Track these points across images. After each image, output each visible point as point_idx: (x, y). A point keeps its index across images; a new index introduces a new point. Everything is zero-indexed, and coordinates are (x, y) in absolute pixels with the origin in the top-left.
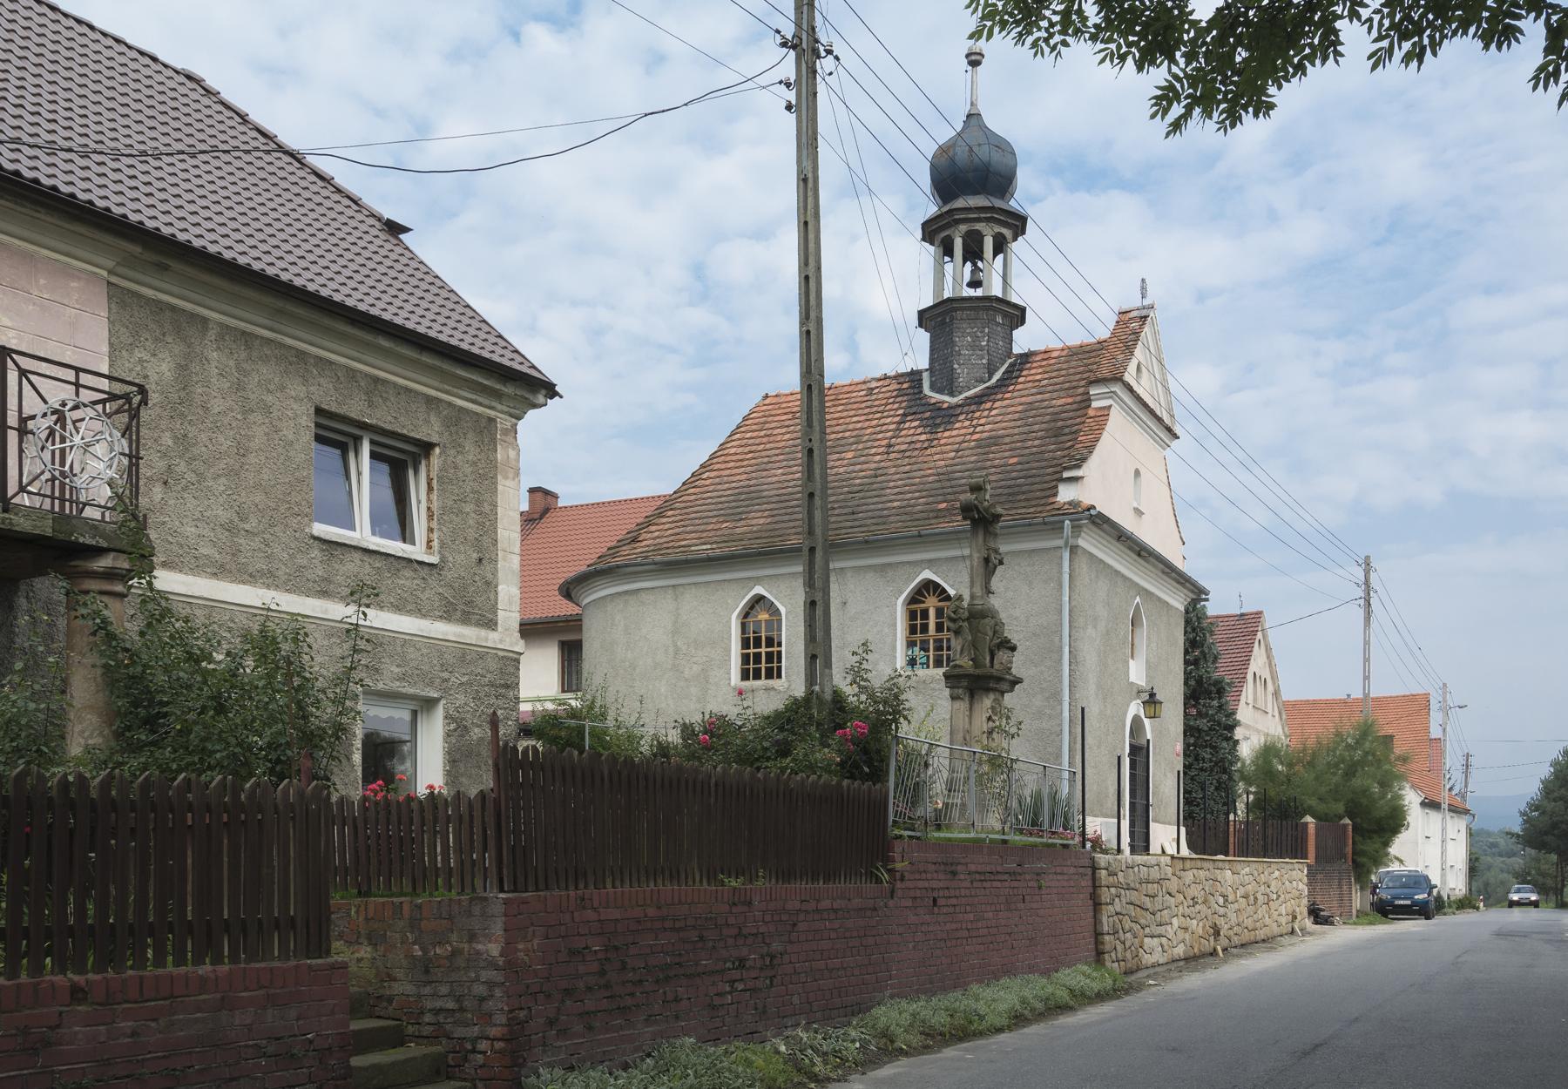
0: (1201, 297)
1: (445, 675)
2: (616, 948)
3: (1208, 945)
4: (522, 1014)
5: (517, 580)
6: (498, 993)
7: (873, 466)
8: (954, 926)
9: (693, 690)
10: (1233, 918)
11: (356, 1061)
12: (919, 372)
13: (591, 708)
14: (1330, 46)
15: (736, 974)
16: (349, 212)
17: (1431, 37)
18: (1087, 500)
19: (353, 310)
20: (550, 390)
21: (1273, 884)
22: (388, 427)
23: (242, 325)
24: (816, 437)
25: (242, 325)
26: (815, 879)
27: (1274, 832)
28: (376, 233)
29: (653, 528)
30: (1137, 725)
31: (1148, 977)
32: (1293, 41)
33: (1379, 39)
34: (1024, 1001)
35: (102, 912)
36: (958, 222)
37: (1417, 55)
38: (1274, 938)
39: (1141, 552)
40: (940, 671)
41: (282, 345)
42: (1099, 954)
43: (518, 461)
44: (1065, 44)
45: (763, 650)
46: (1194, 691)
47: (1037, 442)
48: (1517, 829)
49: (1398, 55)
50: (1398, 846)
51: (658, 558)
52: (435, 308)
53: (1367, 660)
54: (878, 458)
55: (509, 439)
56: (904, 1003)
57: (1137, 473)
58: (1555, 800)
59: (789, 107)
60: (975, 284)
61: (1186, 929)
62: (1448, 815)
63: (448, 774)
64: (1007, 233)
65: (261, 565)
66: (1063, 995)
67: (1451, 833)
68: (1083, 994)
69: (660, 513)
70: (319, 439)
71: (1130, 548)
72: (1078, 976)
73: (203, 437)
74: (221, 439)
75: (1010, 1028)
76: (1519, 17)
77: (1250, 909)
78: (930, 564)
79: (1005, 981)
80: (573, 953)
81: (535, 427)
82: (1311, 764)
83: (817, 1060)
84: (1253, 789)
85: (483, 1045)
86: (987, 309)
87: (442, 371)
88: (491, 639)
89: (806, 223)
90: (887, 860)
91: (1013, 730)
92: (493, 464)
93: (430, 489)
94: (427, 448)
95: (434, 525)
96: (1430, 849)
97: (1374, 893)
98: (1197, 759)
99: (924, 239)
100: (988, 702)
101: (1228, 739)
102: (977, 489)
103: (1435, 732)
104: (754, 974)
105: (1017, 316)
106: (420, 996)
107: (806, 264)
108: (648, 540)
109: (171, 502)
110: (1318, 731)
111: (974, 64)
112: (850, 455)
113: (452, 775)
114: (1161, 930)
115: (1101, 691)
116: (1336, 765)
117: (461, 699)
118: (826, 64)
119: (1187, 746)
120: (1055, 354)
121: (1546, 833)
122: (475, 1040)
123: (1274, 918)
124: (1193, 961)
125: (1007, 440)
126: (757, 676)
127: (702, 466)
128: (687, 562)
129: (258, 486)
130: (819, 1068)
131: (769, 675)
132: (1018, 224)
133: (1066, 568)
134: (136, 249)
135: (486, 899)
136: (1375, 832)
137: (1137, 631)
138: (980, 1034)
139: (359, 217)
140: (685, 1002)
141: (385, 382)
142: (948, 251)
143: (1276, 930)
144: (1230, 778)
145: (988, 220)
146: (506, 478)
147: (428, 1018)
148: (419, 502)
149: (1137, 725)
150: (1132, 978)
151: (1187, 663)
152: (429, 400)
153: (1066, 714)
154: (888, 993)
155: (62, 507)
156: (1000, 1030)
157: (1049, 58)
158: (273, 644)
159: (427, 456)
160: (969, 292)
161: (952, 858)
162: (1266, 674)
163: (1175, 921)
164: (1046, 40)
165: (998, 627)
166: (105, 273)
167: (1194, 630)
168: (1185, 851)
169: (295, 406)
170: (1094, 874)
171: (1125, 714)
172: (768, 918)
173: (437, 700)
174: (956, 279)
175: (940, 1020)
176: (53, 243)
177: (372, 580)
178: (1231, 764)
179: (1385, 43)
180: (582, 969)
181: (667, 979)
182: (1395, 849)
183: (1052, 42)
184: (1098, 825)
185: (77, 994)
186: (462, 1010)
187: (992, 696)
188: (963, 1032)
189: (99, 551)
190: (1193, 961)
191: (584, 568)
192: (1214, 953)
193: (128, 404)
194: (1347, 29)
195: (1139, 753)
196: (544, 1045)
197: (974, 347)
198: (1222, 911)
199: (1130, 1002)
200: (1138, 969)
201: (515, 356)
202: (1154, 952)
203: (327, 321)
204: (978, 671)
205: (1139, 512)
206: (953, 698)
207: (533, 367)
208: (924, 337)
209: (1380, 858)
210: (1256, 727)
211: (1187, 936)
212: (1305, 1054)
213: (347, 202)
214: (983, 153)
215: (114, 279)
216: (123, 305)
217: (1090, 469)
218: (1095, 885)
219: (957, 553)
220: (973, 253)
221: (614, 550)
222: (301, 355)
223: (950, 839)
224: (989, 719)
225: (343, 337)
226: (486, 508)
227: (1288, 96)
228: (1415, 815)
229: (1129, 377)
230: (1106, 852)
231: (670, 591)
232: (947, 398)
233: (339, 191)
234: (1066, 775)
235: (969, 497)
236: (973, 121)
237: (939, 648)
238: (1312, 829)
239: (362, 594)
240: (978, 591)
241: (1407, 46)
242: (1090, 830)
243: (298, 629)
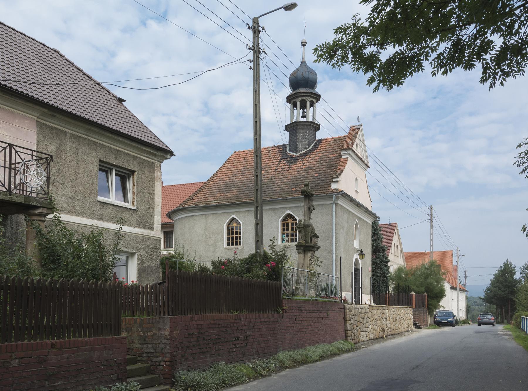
0: (375, 115)
1: (138, 245)
2: (202, 333)
3: (381, 335)
4: (175, 354)
5: (160, 214)
6: (168, 347)
7: (271, 176)
8: (301, 327)
9: (211, 249)
10: (389, 326)
11: (128, 368)
12: (285, 145)
13: (179, 255)
14: (420, 67)
15: (236, 342)
16: (107, 95)
17: (450, 67)
18: (341, 188)
19: (112, 129)
20: (172, 154)
21: (402, 314)
22: (121, 166)
23: (77, 134)
24: (259, 172)
25: (77, 134)
26: (259, 312)
27: (402, 297)
28: (115, 102)
29: (198, 195)
30: (357, 262)
31: (362, 345)
32: (409, 66)
33: (435, 68)
34: (324, 352)
35: (48, 322)
37: (445, 72)
38: (402, 333)
39: (358, 205)
40: (294, 244)
41: (89, 140)
42: (346, 337)
43: (161, 176)
44: (342, 65)
45: (235, 236)
46: (375, 250)
47: (324, 169)
48: (483, 297)
49: (440, 72)
50: (443, 302)
51: (200, 205)
52: (117, 117)
53: (431, 240)
54: (272, 173)
55: (159, 169)
56: (286, 352)
57: (356, 179)
58: (495, 287)
59: (251, 68)
60: (304, 117)
61: (374, 329)
62: (459, 292)
63: (138, 277)
64: (314, 100)
65: (82, 210)
66: (336, 350)
67: (460, 298)
68: (342, 350)
69: (200, 190)
70: (100, 170)
71: (354, 204)
72: (340, 344)
73: (65, 169)
74: (70, 170)
75: (320, 360)
76: (474, 61)
77: (394, 323)
78: (290, 208)
79: (317, 345)
80: (189, 335)
81: (166, 165)
82: (414, 274)
83: (262, 369)
84: (394, 283)
85: (162, 363)
86: (308, 125)
87: (138, 148)
88: (152, 233)
89: (256, 105)
90: (281, 306)
91: (319, 264)
92: (153, 177)
93: (134, 185)
94: (133, 172)
95: (135, 197)
96: (453, 303)
97: (435, 318)
98: (376, 273)
99: (287, 102)
100: (309, 254)
101: (386, 266)
102: (306, 185)
103: (455, 264)
104: (241, 342)
105: (317, 127)
106: (142, 348)
107: (256, 117)
108: (197, 199)
109: (55, 190)
110: (415, 264)
111: (304, 45)
113: (139, 278)
114: (366, 329)
115: (345, 251)
116: (422, 275)
117: (143, 253)
118: (262, 55)
119: (373, 268)
120: (330, 140)
121: (492, 298)
122: (160, 362)
123: (402, 326)
124: (376, 340)
125: (314, 168)
126: (232, 244)
127: (214, 175)
128: (210, 206)
129: (81, 185)
130: (262, 372)
131: (237, 244)
132: (318, 97)
133: (334, 210)
134: (46, 111)
135: (164, 318)
136: (435, 297)
137: (357, 230)
138: (310, 362)
139: (110, 97)
140: (221, 351)
141: (120, 151)
142: (295, 105)
143: (403, 330)
144: (387, 279)
146: (157, 182)
147: (145, 355)
148: (130, 189)
149: (357, 262)
150: (357, 345)
151: (372, 241)
152: (134, 157)
153: (334, 258)
154: (281, 349)
155: (23, 193)
156: (317, 361)
157: (337, 69)
158: (95, 238)
159: (133, 175)
160: (302, 120)
161: (301, 305)
162: (398, 244)
163: (370, 326)
164: (336, 64)
165: (313, 230)
166: (36, 118)
167: (375, 230)
168: (373, 304)
169: (93, 159)
170: (344, 311)
171: (353, 258)
172: (246, 324)
173: (135, 253)
174: (298, 115)
175: (298, 357)
176: (21, 109)
177: (120, 215)
178: (387, 274)
179: (436, 69)
180: (192, 340)
181: (216, 343)
182: (441, 303)
183: (338, 64)
184: (347, 295)
185: (53, 346)
186: (156, 352)
187: (311, 252)
188: (305, 361)
189: (37, 207)
190: (376, 340)
191: (175, 208)
192: (383, 337)
193: (46, 161)
194: (425, 63)
195: (357, 270)
196: (181, 363)
197: (303, 137)
198: (385, 323)
199: (357, 352)
200: (359, 342)
201: (160, 142)
202: (363, 337)
203: (103, 133)
204: (307, 244)
205: (357, 192)
206: (299, 253)
207: (166, 146)
208: (287, 134)
209: (437, 306)
210: (395, 262)
211: (374, 332)
212: (414, 368)
213: (106, 92)
214: (306, 75)
215: (38, 120)
216: (41, 128)
217: (341, 178)
218: (345, 314)
219: (299, 205)
220: (303, 106)
221: (185, 202)
222: (95, 143)
223: (299, 299)
224: (310, 260)
225: (108, 138)
226: (151, 191)
227: (408, 81)
228: (448, 292)
229: (354, 147)
230: (348, 304)
231: (204, 216)
232: (294, 154)
233: (84, 74)
234: (334, 278)
235: (302, 187)
236: (303, 64)
237: (292, 235)
238: (414, 296)
239: (121, 222)
240: (306, 218)
241: (443, 70)
242: (343, 297)
243: (102, 232)
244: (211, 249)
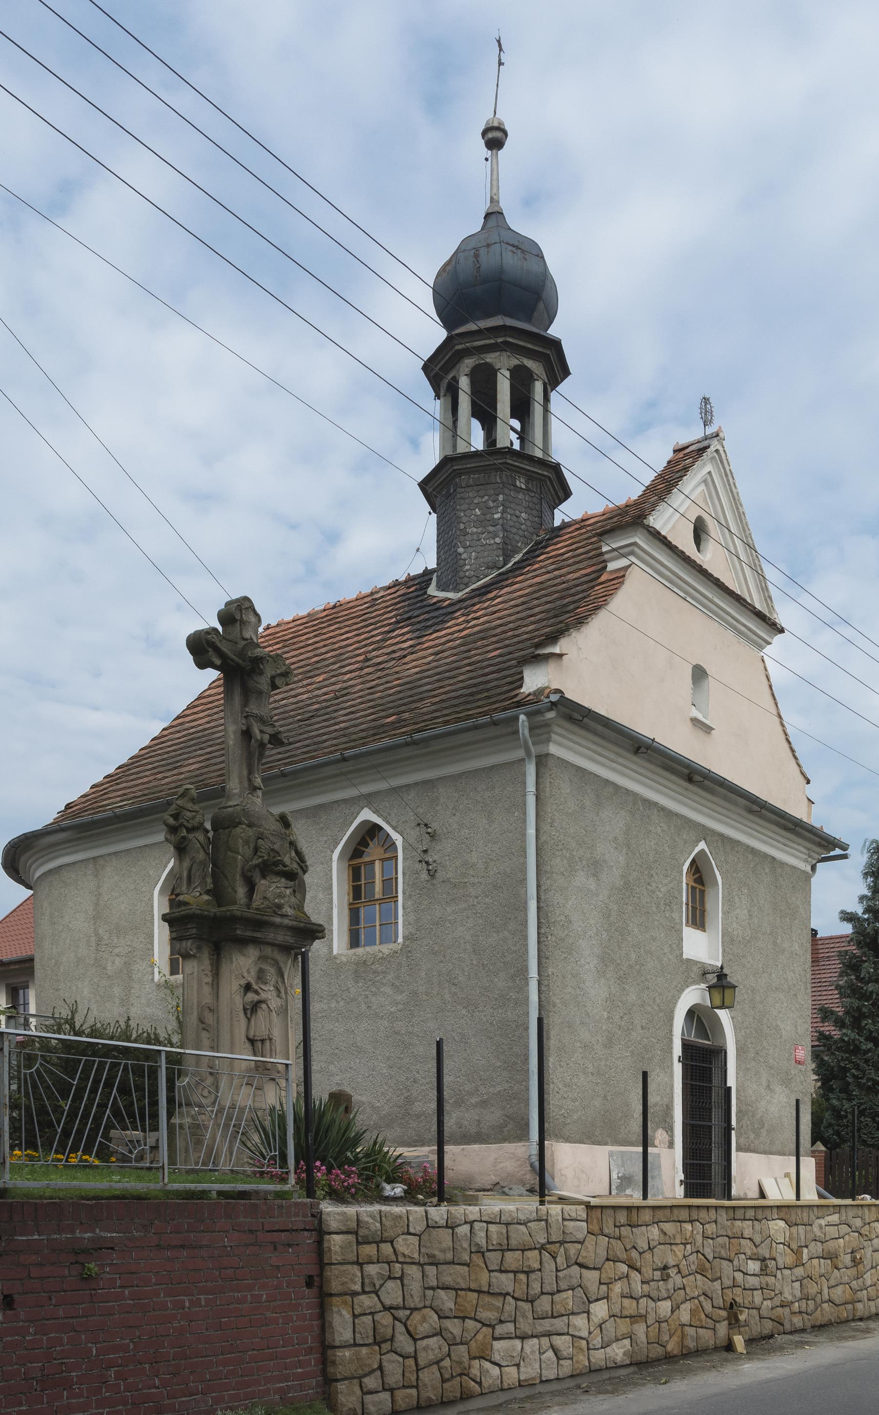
57: (699, 674)
78: (368, 800)
112: (321, 678)
133: (531, 787)
145: (506, 347)
153: (534, 997)
170: (320, 1242)
197: (481, 522)
214: (511, 261)
224: (248, 988)
236: (492, 222)
244: (117, 991)
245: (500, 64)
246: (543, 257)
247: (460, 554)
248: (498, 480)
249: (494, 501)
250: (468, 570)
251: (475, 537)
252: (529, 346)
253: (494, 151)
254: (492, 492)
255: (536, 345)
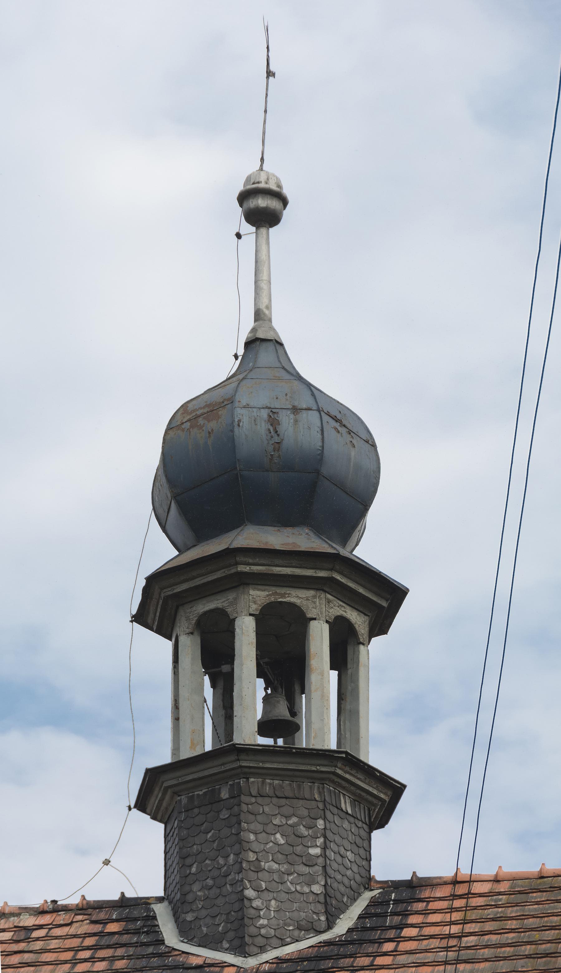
12: (144, 903)
36: (244, 581)
86: (321, 779)
105: (380, 797)
120: (484, 888)
132: (382, 599)
197: (292, 855)
214: (302, 433)
236: (266, 356)
245: (270, 74)
246: (374, 446)
247: (250, 900)
248: (317, 796)
249: (308, 828)
250: (263, 926)
251: (276, 877)
252: (361, 590)
253: (263, 230)
254: (305, 813)
255: (370, 590)
